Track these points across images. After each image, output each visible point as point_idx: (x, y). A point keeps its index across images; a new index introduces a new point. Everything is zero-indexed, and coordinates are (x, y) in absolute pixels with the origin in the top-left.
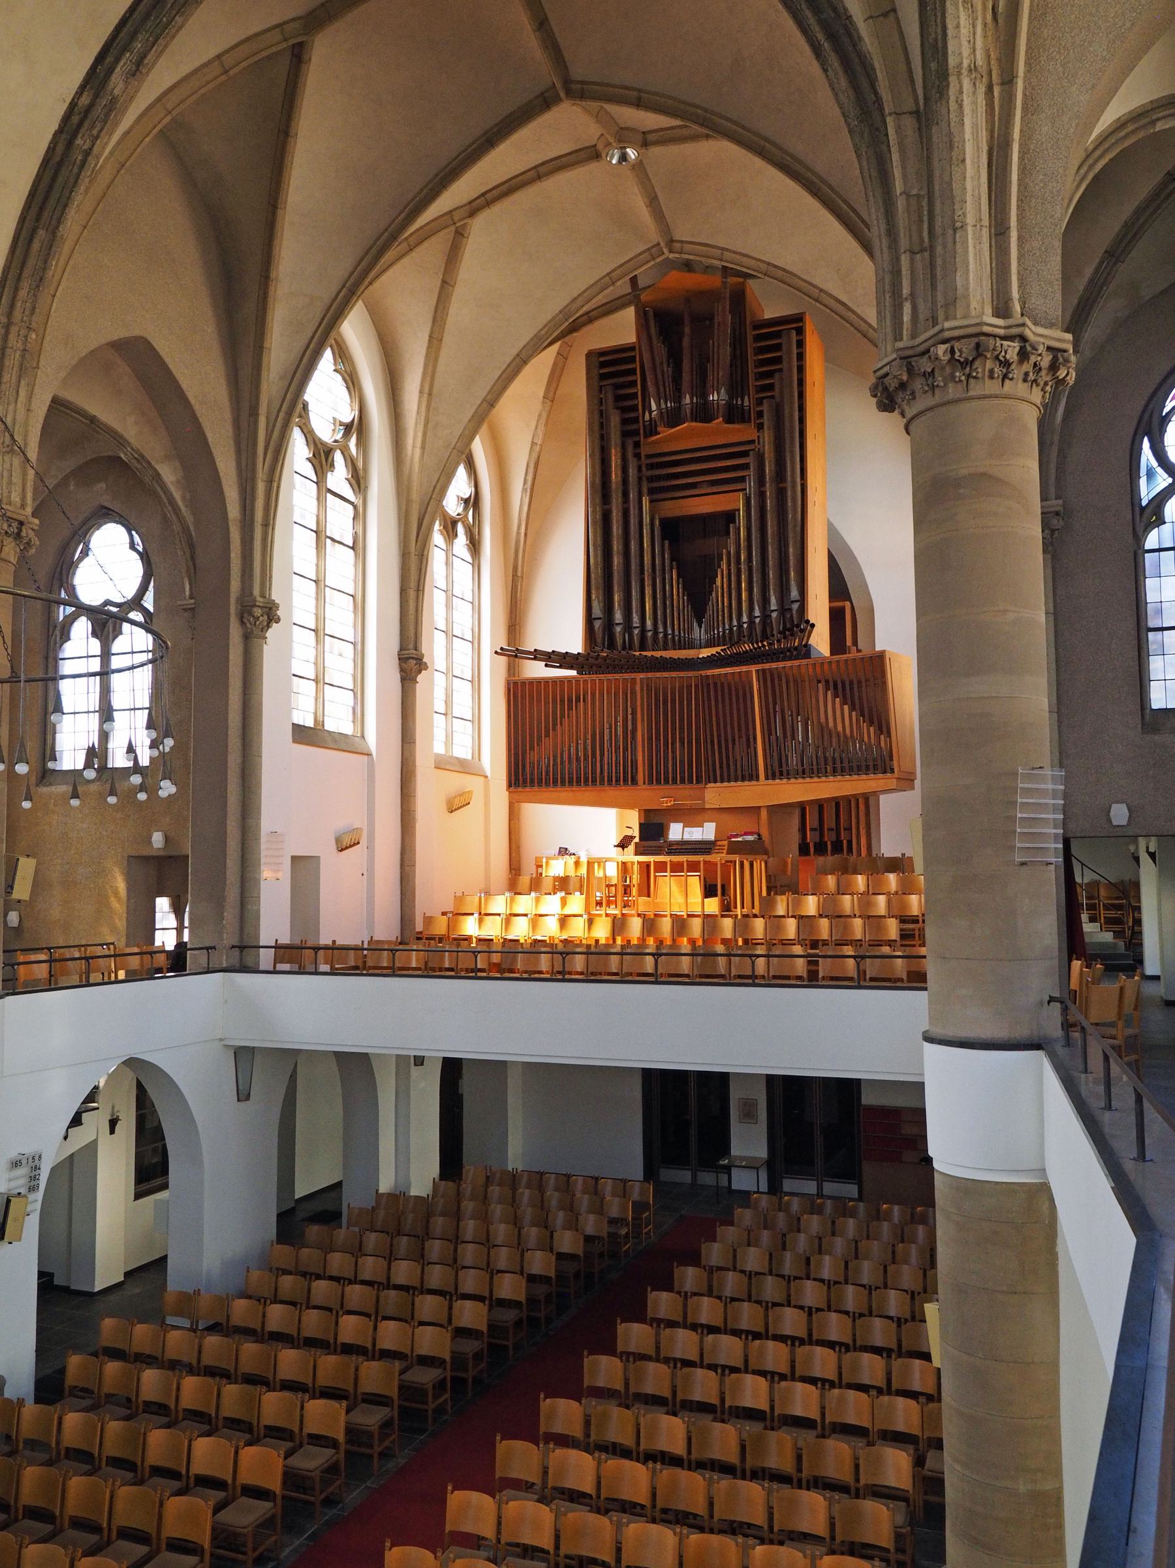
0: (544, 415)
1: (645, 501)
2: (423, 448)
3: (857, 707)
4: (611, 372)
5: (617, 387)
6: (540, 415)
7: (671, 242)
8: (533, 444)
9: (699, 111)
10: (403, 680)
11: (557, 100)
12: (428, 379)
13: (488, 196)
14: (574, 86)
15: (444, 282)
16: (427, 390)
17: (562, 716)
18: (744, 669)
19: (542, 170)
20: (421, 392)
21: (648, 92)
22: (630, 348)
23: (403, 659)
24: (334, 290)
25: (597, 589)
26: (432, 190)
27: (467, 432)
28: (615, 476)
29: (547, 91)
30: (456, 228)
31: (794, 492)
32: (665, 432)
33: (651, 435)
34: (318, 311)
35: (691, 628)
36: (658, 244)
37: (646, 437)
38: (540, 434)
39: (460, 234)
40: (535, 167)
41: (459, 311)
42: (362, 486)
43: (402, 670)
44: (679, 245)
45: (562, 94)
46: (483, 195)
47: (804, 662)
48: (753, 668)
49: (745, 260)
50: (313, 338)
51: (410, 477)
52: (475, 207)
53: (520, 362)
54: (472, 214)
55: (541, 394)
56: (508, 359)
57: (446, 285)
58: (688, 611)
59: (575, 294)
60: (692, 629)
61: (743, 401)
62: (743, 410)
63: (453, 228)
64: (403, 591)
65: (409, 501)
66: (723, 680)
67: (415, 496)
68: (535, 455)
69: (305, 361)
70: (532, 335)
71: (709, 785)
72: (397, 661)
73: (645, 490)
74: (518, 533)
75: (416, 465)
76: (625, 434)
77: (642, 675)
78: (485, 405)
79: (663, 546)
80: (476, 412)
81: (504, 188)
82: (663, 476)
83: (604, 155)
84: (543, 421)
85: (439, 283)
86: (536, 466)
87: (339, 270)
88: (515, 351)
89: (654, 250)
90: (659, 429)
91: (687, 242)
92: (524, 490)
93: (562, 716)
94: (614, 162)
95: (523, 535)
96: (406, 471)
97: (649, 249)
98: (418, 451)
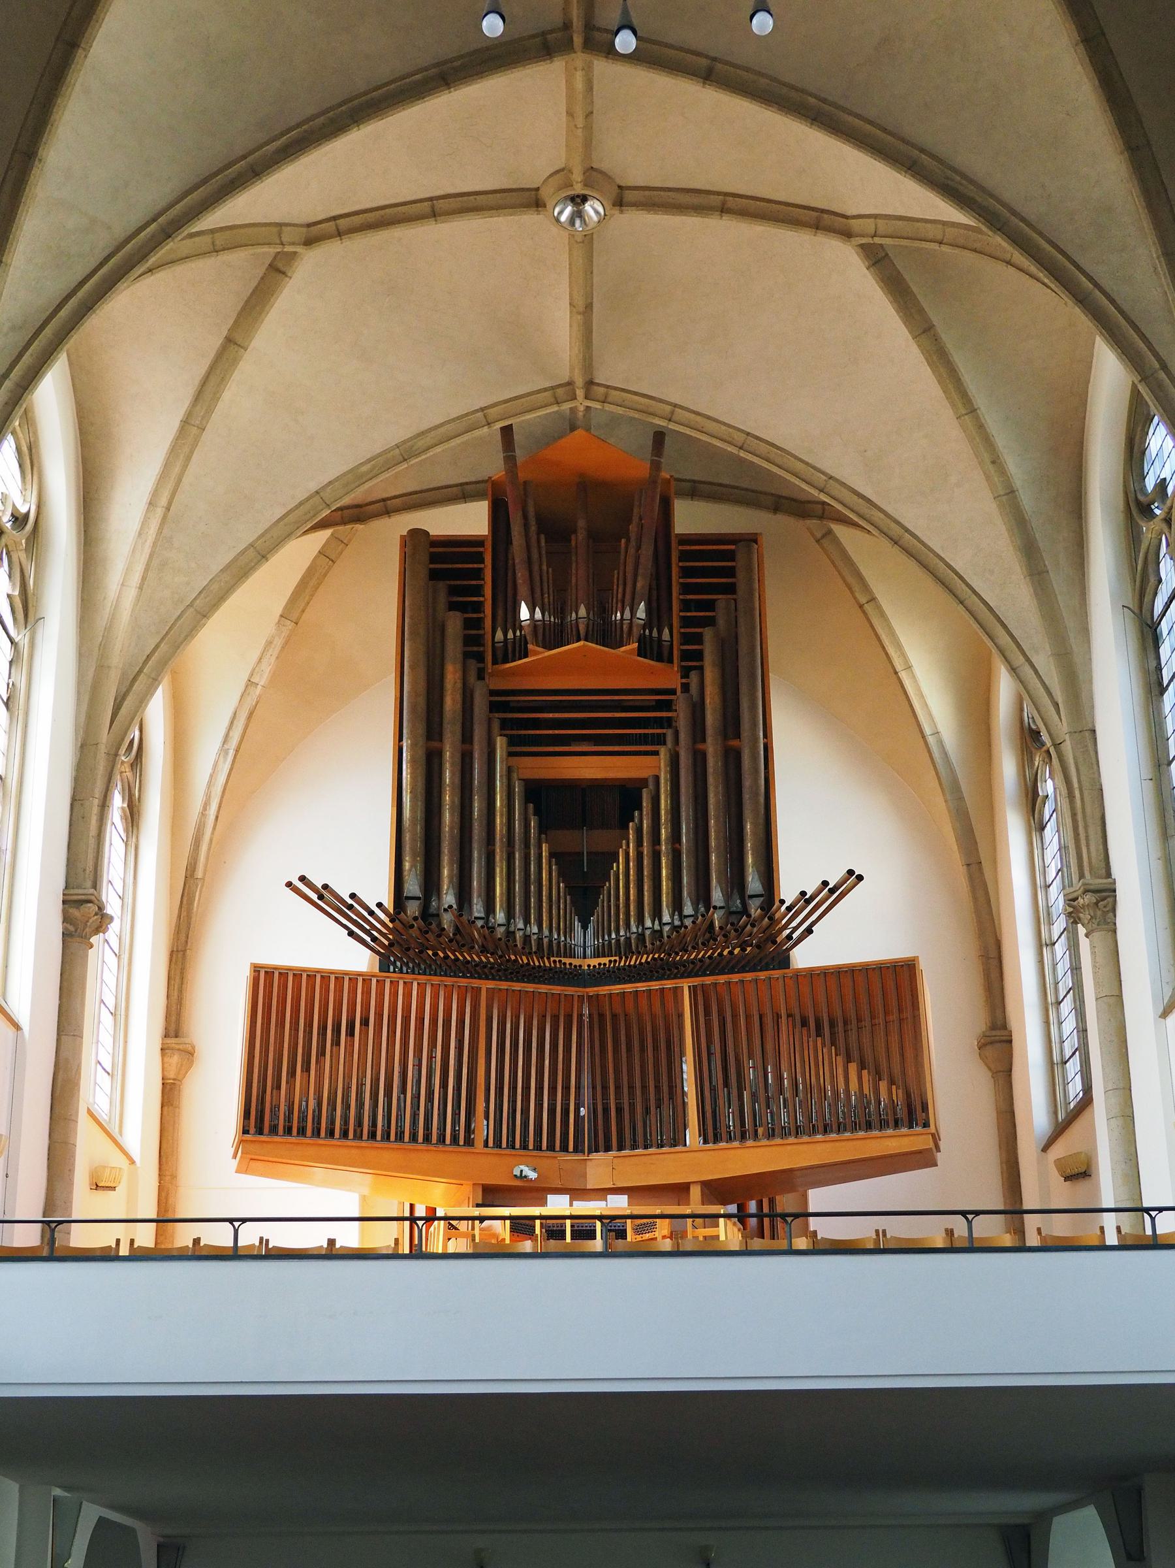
0: (278, 643)
1: (500, 743)
2: (141, 588)
3: (855, 1054)
4: (441, 570)
5: (453, 591)
6: (269, 643)
7: (590, 383)
8: (250, 683)
9: (812, 100)
10: (66, 935)
11: (566, 47)
12: (170, 486)
13: (342, 223)
14: (597, 34)
15: (229, 340)
16: (163, 501)
17: (322, 1053)
18: (668, 984)
19: (440, 204)
20: (151, 504)
21: (727, 63)
22: (477, 542)
23: (69, 902)
24: (135, 219)
25: (414, 855)
26: (332, 121)
27: (215, 587)
28: (451, 703)
29: (551, 32)
30: (277, 255)
31: (754, 758)
32: (539, 654)
33: (506, 661)
34: (102, 242)
35: (569, 930)
36: (570, 383)
37: (495, 662)
38: (267, 668)
39: (277, 270)
40: (431, 199)
41: (239, 397)
42: (31, 619)
43: (66, 919)
44: (602, 390)
45: (578, 40)
46: (335, 218)
47: (776, 974)
48: (685, 985)
49: (711, 426)
50: (82, 284)
51: (109, 629)
52: (315, 234)
53: (240, 570)
54: (309, 242)
55: (278, 609)
56: (301, 495)
57: (232, 346)
58: (566, 902)
59: (425, 426)
60: (572, 929)
61: (660, 632)
62: (660, 645)
63: (272, 250)
64: (76, 801)
65: (102, 668)
66: (618, 1009)
67: (117, 658)
68: (250, 702)
69: (63, 313)
70: (345, 468)
71: (594, 1156)
72: (59, 906)
73: (496, 726)
74: (203, 814)
75: (125, 616)
76: (467, 655)
77: (491, 984)
78: (251, 553)
79: (526, 809)
80: (235, 559)
81: (370, 217)
82: (528, 721)
83: (549, 206)
84: (275, 651)
85: (217, 342)
86: (250, 717)
87: (151, 194)
88: (313, 486)
89: (560, 391)
90: (530, 646)
91: (616, 389)
92: (223, 750)
93: (322, 1053)
94: (563, 218)
95: (212, 818)
96: (101, 622)
97: (553, 388)
98: (131, 593)
